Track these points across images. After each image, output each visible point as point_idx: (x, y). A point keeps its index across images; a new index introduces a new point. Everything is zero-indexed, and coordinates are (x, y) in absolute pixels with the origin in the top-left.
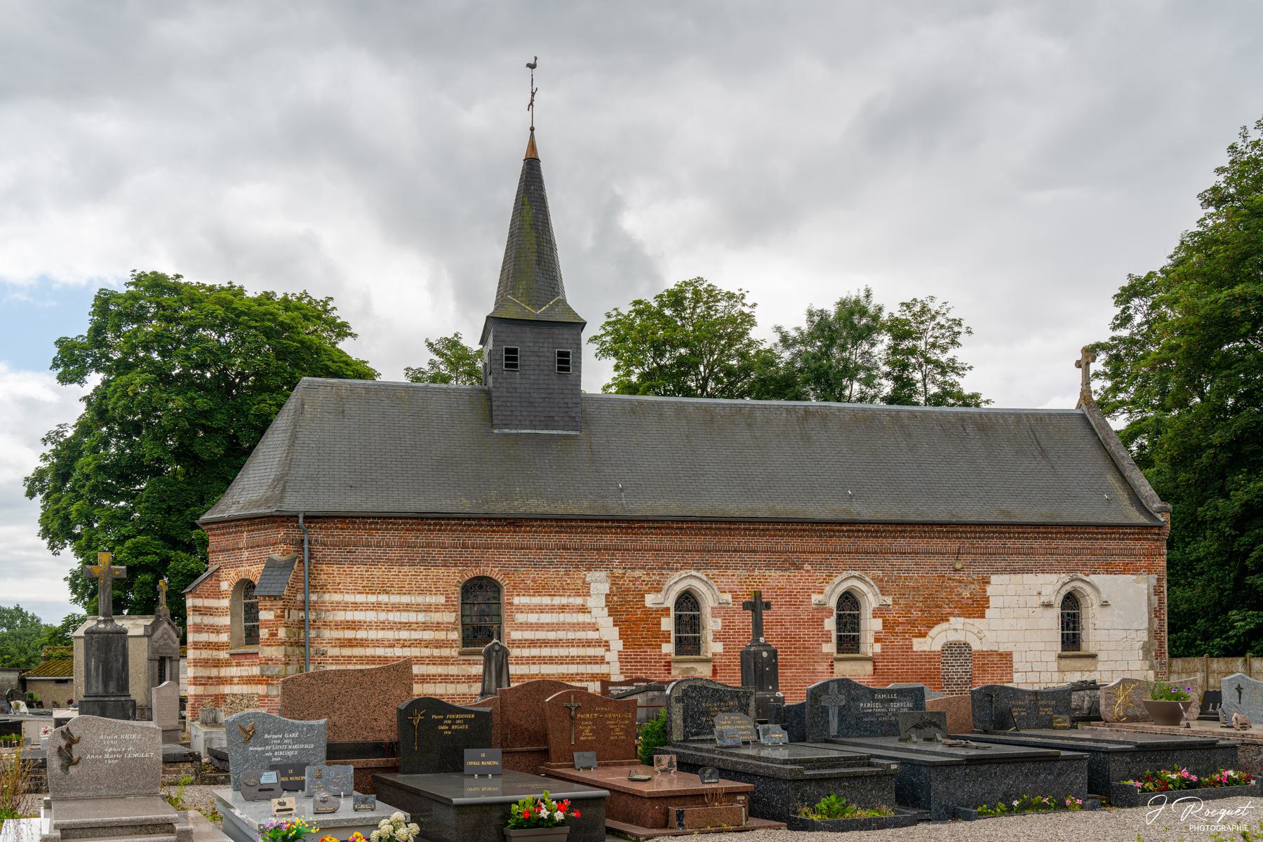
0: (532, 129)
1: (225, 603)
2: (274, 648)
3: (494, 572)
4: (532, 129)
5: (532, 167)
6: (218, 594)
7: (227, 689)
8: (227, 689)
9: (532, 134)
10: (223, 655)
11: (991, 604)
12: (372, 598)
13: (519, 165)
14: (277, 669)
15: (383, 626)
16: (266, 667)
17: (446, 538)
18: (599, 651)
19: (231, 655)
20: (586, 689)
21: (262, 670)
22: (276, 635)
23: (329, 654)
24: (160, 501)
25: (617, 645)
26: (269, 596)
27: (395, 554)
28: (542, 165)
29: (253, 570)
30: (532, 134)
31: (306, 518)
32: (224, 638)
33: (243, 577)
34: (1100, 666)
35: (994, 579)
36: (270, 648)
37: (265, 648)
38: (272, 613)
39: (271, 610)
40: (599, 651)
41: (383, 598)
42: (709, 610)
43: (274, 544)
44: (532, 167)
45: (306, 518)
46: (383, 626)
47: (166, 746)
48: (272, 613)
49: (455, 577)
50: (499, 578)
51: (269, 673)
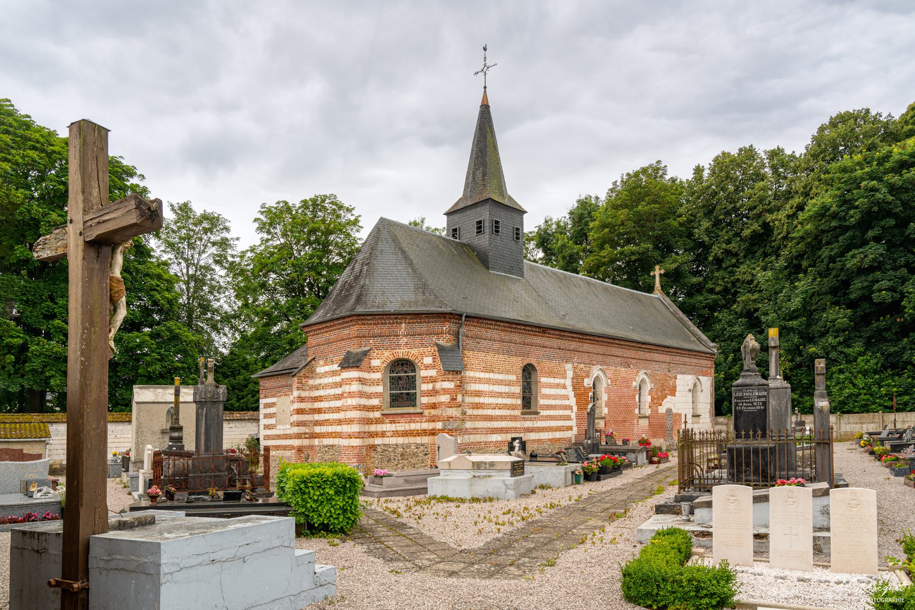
0: (485, 88)
1: (378, 376)
2: (454, 409)
3: (534, 362)
4: (485, 88)
5: (485, 110)
6: (371, 369)
7: (378, 441)
8: (378, 441)
9: (485, 91)
10: (377, 414)
11: (677, 389)
12: (487, 375)
13: (478, 110)
14: (456, 424)
15: (492, 394)
16: (447, 423)
17: (516, 337)
18: (567, 412)
19: (383, 415)
20: (21, 450)
21: (445, 425)
22: (455, 399)
23: (468, 414)
24: (22, 294)
25: (575, 409)
26: (453, 371)
27: (496, 345)
28: (491, 109)
29: (413, 352)
30: (485, 91)
31: (466, 317)
32: (375, 402)
33: (401, 356)
34: (701, 421)
35: (679, 376)
36: (451, 409)
37: (448, 409)
38: (453, 383)
39: (452, 381)
40: (567, 412)
41: (491, 375)
42: (603, 389)
43: (438, 334)
44: (485, 110)
45: (466, 317)
46: (492, 394)
47: (425, 486)
48: (453, 383)
49: (518, 363)
50: (536, 365)
51: (450, 427)
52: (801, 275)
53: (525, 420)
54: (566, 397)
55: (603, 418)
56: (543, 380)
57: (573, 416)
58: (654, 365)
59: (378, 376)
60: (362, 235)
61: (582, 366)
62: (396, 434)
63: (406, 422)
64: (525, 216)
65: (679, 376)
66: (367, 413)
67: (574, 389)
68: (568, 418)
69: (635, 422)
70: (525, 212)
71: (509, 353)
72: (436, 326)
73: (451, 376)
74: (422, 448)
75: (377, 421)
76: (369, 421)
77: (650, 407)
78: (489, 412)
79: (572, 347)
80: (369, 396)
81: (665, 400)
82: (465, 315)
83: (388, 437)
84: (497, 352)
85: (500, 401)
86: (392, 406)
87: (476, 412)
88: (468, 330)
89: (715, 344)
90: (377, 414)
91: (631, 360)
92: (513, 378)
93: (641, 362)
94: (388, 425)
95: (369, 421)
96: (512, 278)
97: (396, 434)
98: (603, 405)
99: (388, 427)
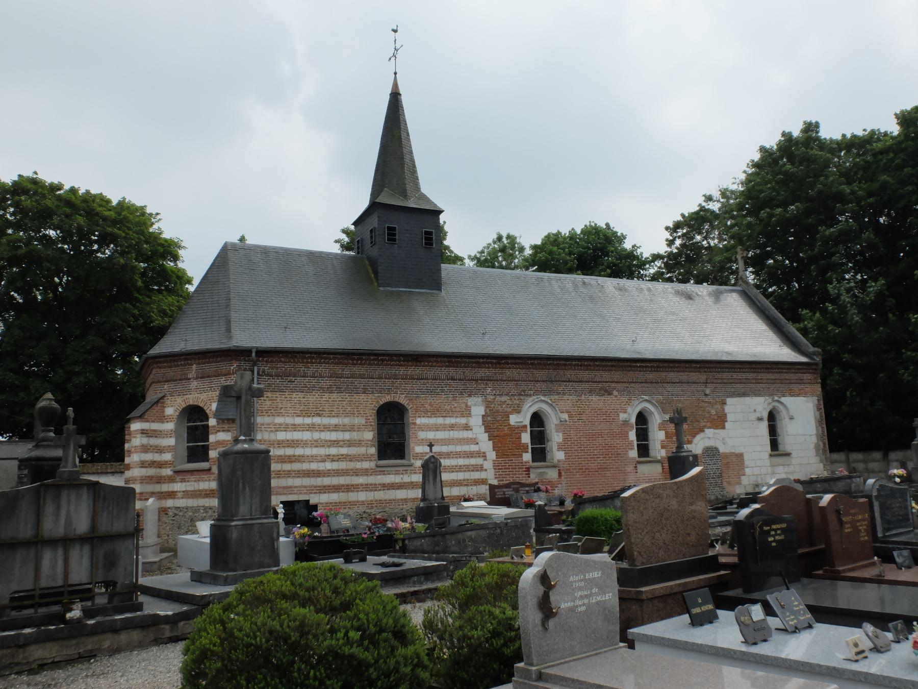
0: (395, 73)
1: (170, 426)
3: (402, 399)
4: (395, 73)
6: (162, 419)
8: (169, 503)
9: (395, 77)
10: (168, 472)
12: (308, 421)
13: (387, 99)
15: (316, 444)
18: (479, 461)
19: (175, 472)
25: (492, 455)
29: (202, 397)
30: (395, 77)
32: (167, 457)
34: (794, 461)
35: (729, 401)
39: (228, 431)
40: (479, 461)
46: (316, 444)
49: (371, 402)
52: (647, 266)
53: (383, 473)
54: (475, 442)
55: (555, 467)
56: (419, 421)
57: (488, 465)
58: (670, 388)
59: (170, 426)
60: (682, 219)
61: (504, 398)
62: (187, 494)
63: (195, 481)
64: (442, 218)
65: (729, 401)
66: (158, 470)
67: (488, 429)
68: (480, 468)
69: (630, 468)
70: (441, 212)
71: (352, 390)
72: (224, 366)
73: (226, 426)
74: (210, 511)
75: (171, 480)
76: (160, 480)
77: (663, 447)
78: (314, 466)
79: (479, 376)
80: (160, 450)
81: (701, 435)
82: (254, 351)
83: (178, 498)
84: (330, 390)
85: (333, 451)
86: (189, 461)
87: (287, 467)
88: (272, 368)
89: (816, 349)
90: (168, 472)
91: (613, 385)
92: (359, 421)
93: (637, 385)
94: (179, 484)
95: (160, 480)
96: (398, 293)
97: (187, 494)
98: (555, 448)
99: (178, 487)
